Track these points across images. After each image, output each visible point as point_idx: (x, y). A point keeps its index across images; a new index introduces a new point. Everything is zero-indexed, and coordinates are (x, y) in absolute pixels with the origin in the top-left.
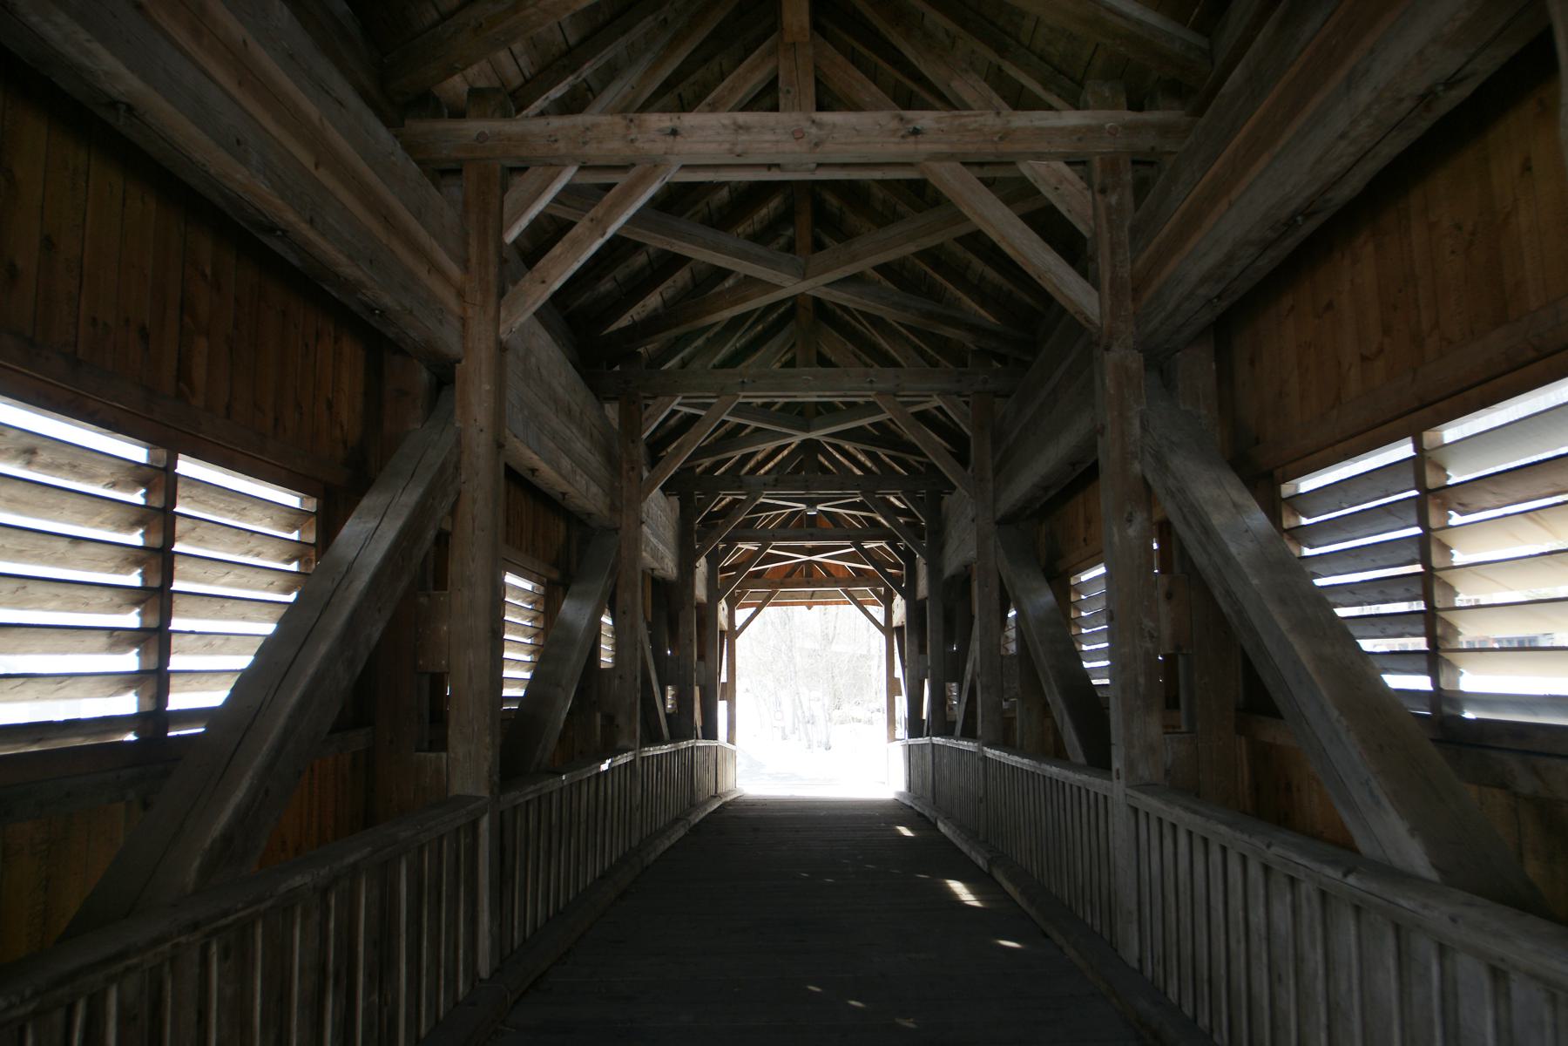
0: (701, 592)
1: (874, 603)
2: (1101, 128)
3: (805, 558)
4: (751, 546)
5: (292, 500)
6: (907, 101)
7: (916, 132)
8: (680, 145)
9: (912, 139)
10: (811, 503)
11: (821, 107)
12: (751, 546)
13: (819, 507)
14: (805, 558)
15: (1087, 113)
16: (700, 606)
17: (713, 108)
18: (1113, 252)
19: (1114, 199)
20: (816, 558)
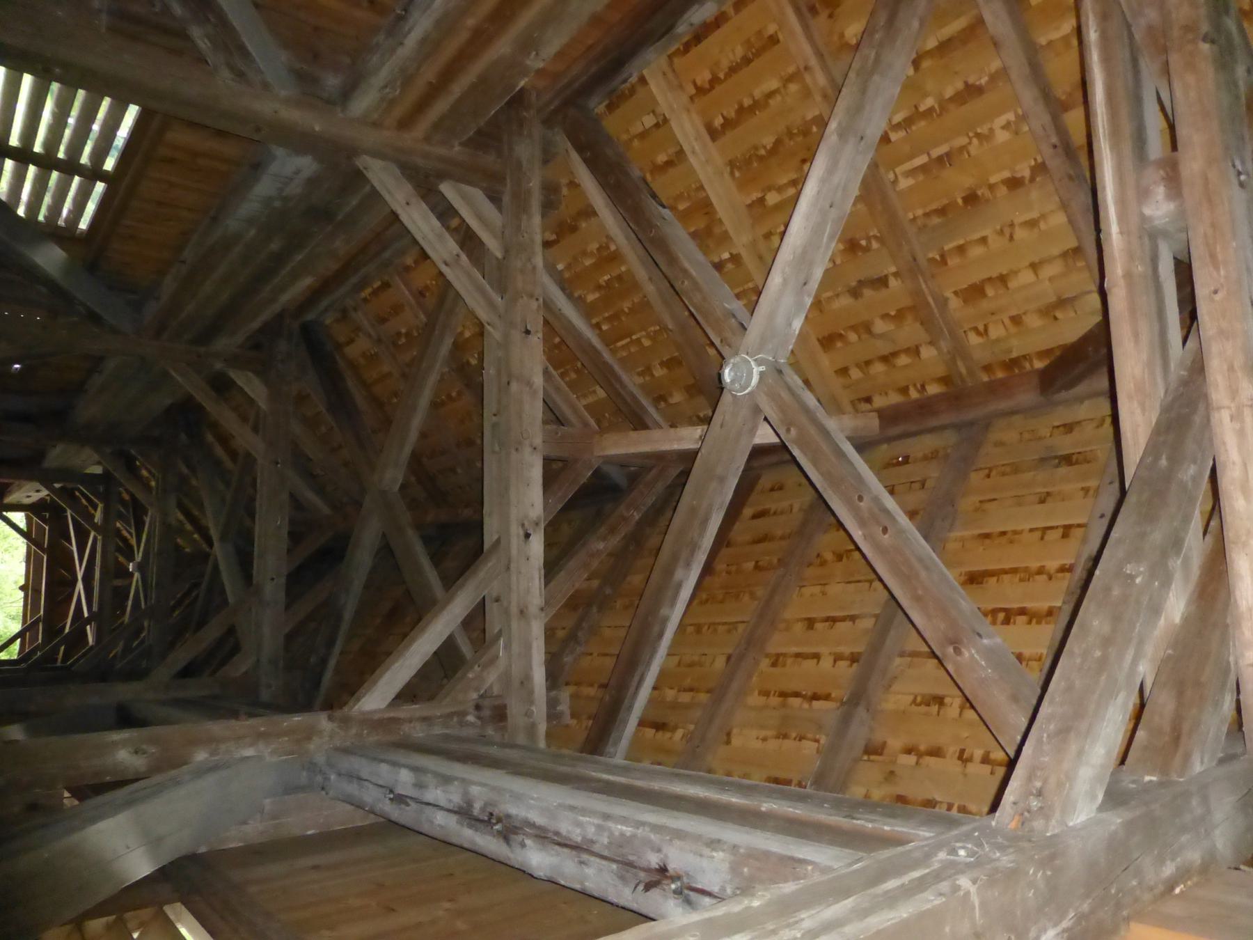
0: (57, 455)
1: (22, 645)
2: (532, 702)
3: (80, 575)
4: (98, 517)
5: (83, 225)
6: (552, 530)
7: (527, 536)
8: (517, 335)
9: (522, 533)
10: (141, 567)
11: (547, 461)
12: (98, 517)
13: (137, 575)
14: (80, 575)
15: (544, 691)
16: (40, 455)
17: (546, 372)
18: (425, 719)
19: (471, 718)
20: (80, 586)
